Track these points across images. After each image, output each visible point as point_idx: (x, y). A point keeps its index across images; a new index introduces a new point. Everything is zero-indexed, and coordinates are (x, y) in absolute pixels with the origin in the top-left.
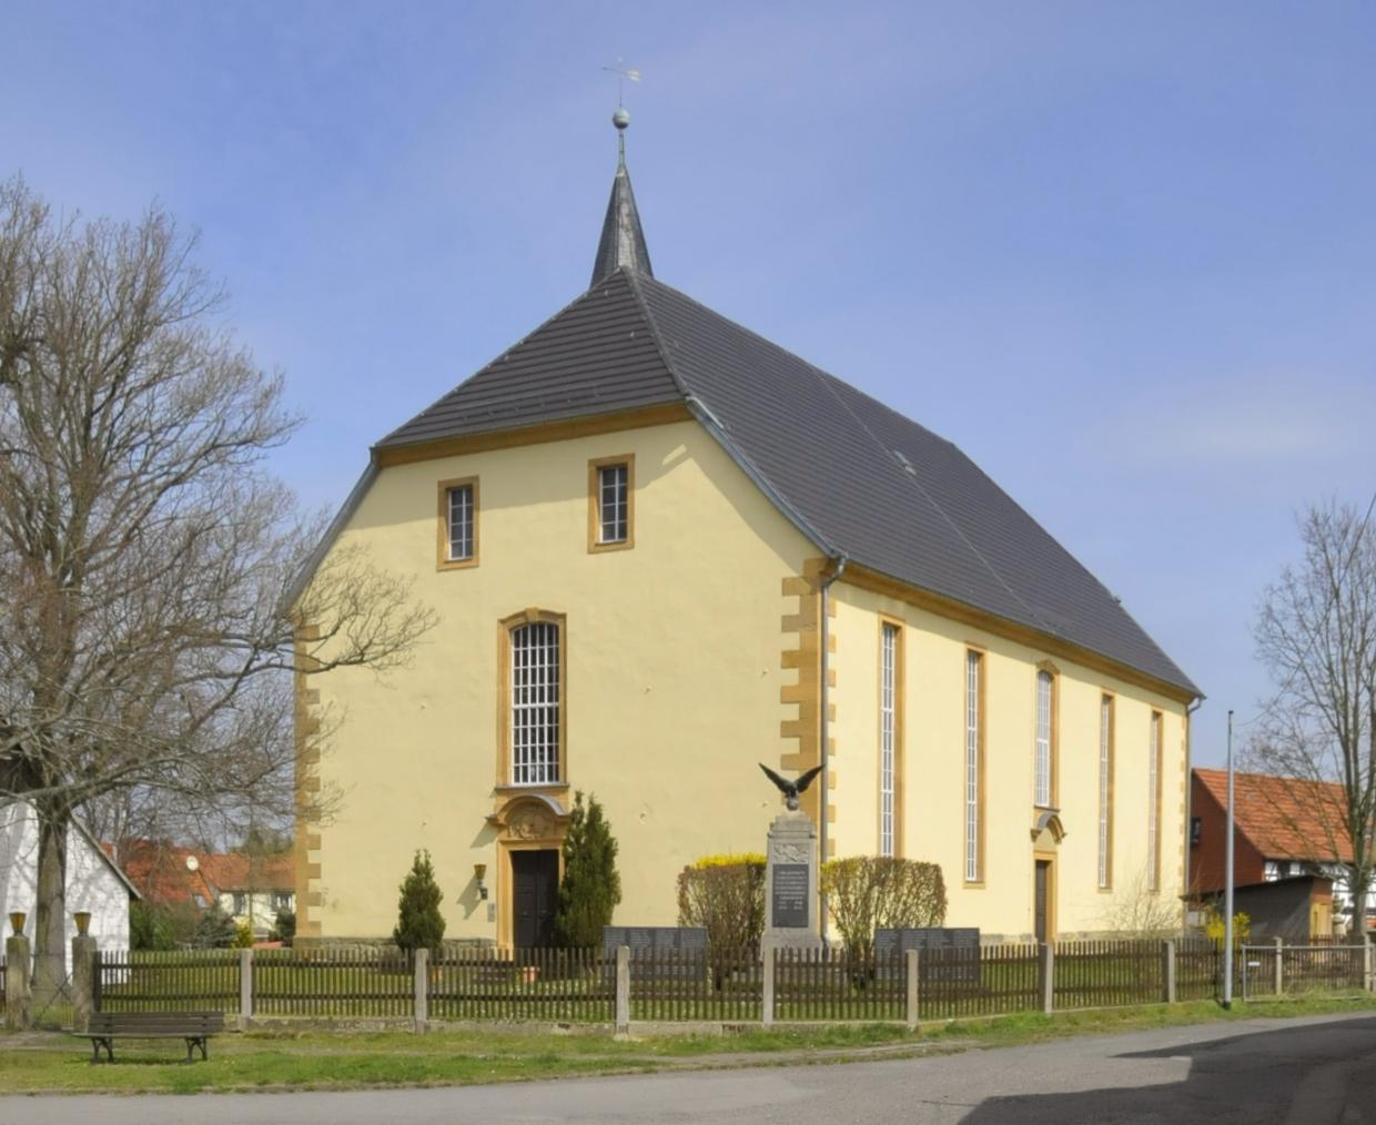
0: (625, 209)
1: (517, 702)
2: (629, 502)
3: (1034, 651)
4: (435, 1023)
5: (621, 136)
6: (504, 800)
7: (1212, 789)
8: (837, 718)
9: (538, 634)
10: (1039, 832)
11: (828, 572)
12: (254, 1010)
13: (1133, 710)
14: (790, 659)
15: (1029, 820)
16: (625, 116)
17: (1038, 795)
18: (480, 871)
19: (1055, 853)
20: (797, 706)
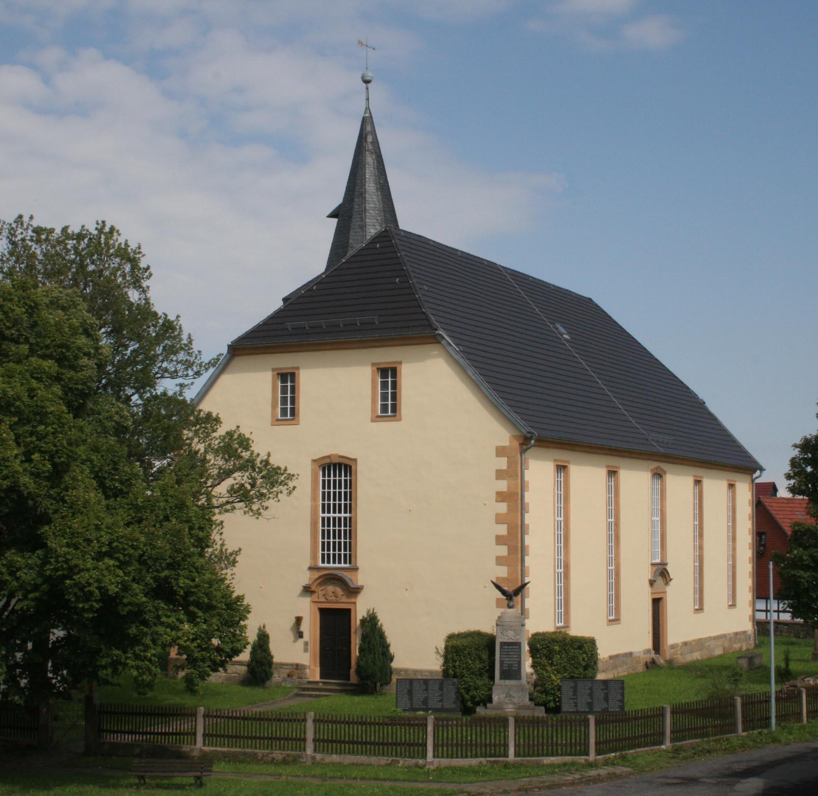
0: (370, 139)
1: (323, 512)
2: (398, 391)
3: (649, 462)
4: (319, 756)
5: (367, 88)
6: (317, 575)
7: (773, 512)
8: (530, 533)
9: (338, 472)
10: (655, 581)
11: (525, 442)
12: (204, 745)
13: (715, 487)
14: (501, 497)
15: (647, 574)
16: (369, 75)
17: (653, 556)
18: (299, 620)
19: (665, 592)
20: (506, 526)
